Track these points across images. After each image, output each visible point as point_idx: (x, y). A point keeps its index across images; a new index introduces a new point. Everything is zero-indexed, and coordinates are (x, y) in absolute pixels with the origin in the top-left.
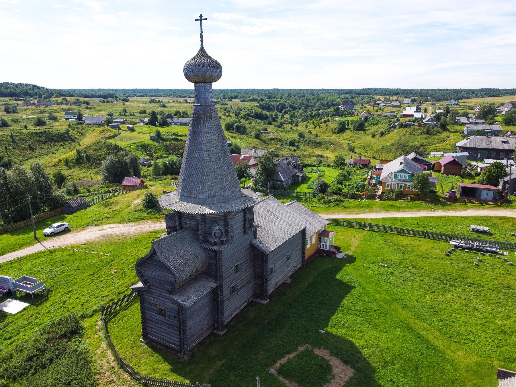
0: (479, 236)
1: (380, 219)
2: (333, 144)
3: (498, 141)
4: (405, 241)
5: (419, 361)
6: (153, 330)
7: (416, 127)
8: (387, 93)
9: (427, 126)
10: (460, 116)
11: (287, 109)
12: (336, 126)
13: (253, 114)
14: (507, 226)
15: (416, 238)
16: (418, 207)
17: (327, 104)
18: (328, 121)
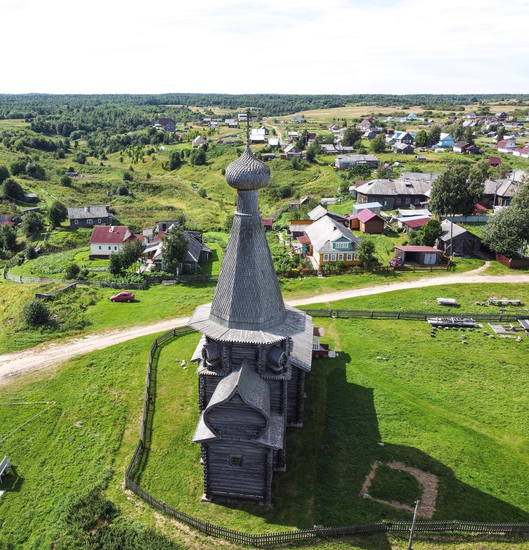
0: (449, 310)
1: (339, 301)
2: (177, 188)
3: (402, 185)
4: (384, 325)
5: (479, 453)
6: (222, 484)
7: (279, 160)
8: (204, 102)
9: (293, 159)
10: (325, 143)
11: (78, 132)
12: (167, 159)
13: (31, 142)
14: (467, 294)
15: (391, 321)
16: (368, 281)
17: (131, 121)
18: (153, 151)
